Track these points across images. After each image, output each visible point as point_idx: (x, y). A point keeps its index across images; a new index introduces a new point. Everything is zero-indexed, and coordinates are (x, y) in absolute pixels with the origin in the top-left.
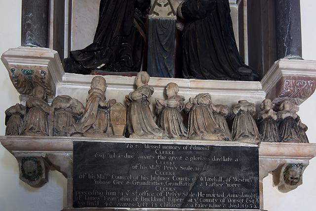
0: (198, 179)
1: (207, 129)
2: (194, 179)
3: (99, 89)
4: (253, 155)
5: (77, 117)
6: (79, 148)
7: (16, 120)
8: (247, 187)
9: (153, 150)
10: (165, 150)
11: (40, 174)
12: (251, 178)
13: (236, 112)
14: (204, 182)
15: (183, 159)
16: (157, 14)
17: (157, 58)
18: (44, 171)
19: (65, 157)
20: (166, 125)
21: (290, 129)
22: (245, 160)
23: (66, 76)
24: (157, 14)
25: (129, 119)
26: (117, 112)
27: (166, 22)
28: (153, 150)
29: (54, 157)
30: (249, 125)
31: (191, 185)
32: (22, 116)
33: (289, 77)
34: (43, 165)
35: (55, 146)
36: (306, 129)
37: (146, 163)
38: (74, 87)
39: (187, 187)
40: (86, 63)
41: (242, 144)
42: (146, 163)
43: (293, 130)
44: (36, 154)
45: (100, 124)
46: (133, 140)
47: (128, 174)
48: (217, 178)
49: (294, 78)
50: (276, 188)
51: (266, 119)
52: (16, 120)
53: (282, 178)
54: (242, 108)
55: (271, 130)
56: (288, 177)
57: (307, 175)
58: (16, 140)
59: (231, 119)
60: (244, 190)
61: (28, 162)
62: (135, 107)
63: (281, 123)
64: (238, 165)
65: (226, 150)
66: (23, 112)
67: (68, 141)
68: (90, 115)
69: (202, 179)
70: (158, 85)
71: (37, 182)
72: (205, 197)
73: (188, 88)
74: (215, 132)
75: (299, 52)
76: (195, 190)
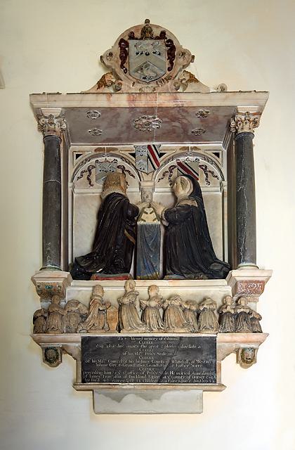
0: (171, 362)
1: (177, 325)
2: (167, 362)
3: (99, 296)
4: (212, 342)
5: (84, 317)
6: (85, 341)
7: (41, 321)
8: (207, 367)
9: (138, 341)
10: (148, 341)
11: (57, 358)
12: (210, 360)
13: (202, 309)
14: (175, 364)
15: (160, 347)
16: (145, 221)
17: (144, 257)
18: (60, 357)
19: (76, 346)
20: (148, 321)
21: (249, 321)
22: (206, 347)
23: (74, 283)
24: (145, 221)
25: (120, 317)
26: (112, 312)
27: (152, 226)
28: (138, 341)
29: (67, 346)
30: (210, 319)
31: (166, 366)
32: (45, 318)
33: (242, 282)
34: (59, 352)
35: (69, 340)
36: (260, 318)
37: (133, 351)
38: (80, 290)
39: (162, 367)
40: (88, 267)
41: (203, 335)
42: (133, 351)
43: (245, 323)
44: (55, 345)
45: (99, 323)
46: (123, 334)
47: (120, 359)
48: (185, 360)
49: (246, 282)
50: (155, 401)
51: (226, 313)
52: (41, 321)
53: (240, 358)
54: (205, 306)
55: (228, 322)
56: (246, 358)
57: (259, 355)
58: (43, 337)
59: (198, 311)
60: (205, 369)
61: (50, 351)
62: (124, 308)
63: (237, 316)
64: (200, 351)
65: (191, 340)
66: (46, 315)
67: (78, 337)
68: (92, 317)
69: (173, 362)
70: (142, 287)
71: (55, 364)
72: (175, 375)
73: (170, 288)
74: (183, 326)
75: (253, 259)
76: (168, 369)
